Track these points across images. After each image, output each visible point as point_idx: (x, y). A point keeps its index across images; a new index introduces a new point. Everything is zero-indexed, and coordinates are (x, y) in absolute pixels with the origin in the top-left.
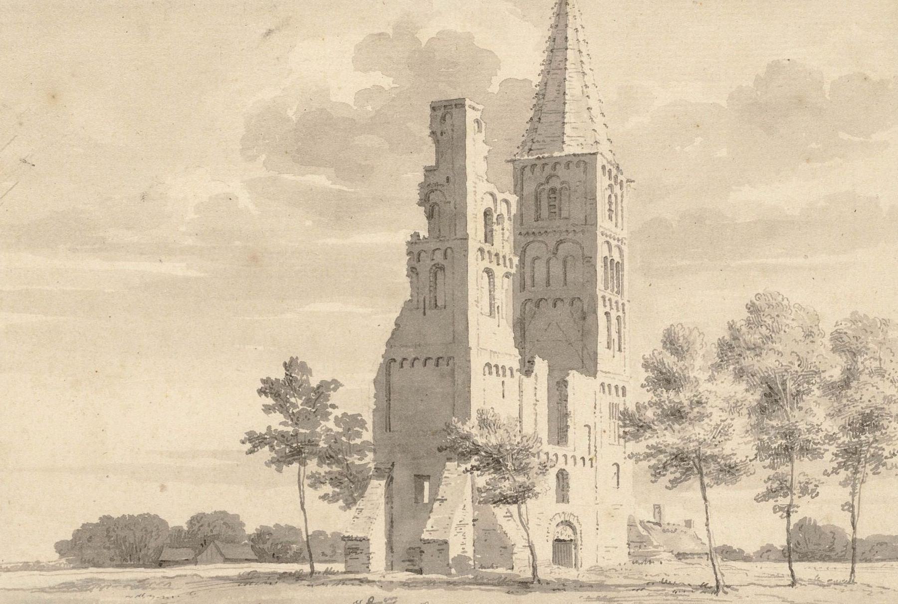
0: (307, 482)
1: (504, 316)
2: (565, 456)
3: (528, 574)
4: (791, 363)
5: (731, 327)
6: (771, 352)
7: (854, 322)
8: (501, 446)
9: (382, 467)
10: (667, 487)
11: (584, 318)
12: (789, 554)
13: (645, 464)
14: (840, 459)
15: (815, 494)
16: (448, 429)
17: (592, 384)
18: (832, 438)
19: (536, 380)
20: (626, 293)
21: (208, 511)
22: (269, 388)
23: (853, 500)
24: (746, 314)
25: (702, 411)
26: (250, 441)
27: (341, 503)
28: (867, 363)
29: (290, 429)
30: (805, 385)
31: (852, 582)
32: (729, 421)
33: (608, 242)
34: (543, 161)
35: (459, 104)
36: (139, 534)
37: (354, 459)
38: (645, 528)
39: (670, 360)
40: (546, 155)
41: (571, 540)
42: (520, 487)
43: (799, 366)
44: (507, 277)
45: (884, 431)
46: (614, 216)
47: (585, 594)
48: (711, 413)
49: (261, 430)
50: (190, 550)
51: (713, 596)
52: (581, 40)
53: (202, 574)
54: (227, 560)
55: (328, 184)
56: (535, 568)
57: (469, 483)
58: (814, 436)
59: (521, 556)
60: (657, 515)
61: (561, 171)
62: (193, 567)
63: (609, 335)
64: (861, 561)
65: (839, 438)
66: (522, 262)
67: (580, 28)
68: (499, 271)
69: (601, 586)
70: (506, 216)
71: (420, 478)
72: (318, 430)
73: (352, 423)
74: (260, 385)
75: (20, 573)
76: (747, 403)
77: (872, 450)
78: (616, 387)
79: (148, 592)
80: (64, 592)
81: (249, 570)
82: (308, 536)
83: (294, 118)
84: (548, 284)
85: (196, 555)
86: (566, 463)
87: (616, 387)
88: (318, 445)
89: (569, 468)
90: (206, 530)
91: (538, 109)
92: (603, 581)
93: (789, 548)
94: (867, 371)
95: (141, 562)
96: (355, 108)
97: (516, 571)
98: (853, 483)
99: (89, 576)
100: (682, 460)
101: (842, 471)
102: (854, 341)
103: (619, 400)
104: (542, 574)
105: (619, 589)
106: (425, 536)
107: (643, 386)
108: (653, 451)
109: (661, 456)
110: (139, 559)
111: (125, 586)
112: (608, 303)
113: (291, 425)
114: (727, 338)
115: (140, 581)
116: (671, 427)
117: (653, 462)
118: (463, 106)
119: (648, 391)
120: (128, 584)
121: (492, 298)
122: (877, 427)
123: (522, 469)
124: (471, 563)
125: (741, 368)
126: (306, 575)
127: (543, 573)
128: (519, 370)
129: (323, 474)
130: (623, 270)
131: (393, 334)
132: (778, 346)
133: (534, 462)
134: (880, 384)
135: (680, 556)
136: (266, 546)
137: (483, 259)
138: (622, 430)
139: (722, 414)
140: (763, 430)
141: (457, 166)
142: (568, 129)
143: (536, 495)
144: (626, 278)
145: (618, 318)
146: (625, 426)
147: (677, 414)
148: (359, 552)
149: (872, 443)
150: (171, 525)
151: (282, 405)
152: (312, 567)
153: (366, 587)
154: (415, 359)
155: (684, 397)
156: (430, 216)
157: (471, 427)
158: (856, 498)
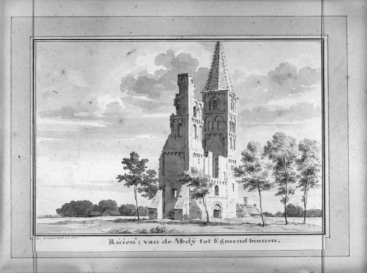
0: (137, 191)
1: (199, 139)
2: (218, 181)
3: (206, 220)
4: (286, 153)
5: (268, 143)
6: (280, 150)
7: (305, 141)
8: (198, 178)
9: (162, 186)
10: (248, 191)
11: (224, 140)
12: (285, 215)
13: (242, 184)
14: (301, 183)
15: (293, 193)
16: (183, 174)
17: (226, 160)
18: (298, 176)
19: (209, 158)
20: (236, 132)
21: (106, 200)
22: (125, 161)
23: (305, 195)
24: (272, 139)
25: (259, 168)
26: (119, 178)
27: (148, 197)
28: (309, 154)
29: (132, 174)
30: (291, 160)
31: (304, 223)
32: (267, 171)
33: (231, 117)
34: (212, 93)
35: (186, 75)
36: (83, 207)
37: (152, 184)
38: (242, 206)
39: (249, 152)
40: (212, 91)
41: (219, 210)
42: (204, 190)
43: (289, 154)
44: (200, 127)
45: (314, 175)
46: (233, 109)
47: (223, 226)
48: (262, 169)
49: (123, 174)
50: (99, 212)
51: (262, 227)
52: (223, 56)
53: (103, 219)
54: (111, 215)
55: (146, 99)
56: (208, 218)
57: (188, 189)
58: (293, 176)
59: (204, 215)
60: (245, 203)
61: (217, 95)
62: (100, 217)
63: (231, 145)
64: (307, 217)
65: (301, 177)
66: (205, 122)
67: (223, 53)
68: (198, 125)
69: (228, 224)
70: (200, 109)
71: (173, 190)
72: (141, 175)
73: (152, 173)
74: (123, 160)
75: (45, 219)
76: (273, 166)
77: (311, 180)
78: (233, 161)
79: (86, 225)
80: (59, 224)
81: (118, 218)
82: (137, 208)
83: (136, 79)
84: (213, 129)
85: (102, 213)
86: (218, 183)
87: (233, 161)
88: (141, 179)
89: (219, 185)
90: (105, 205)
91: (210, 77)
92: (229, 223)
93: (285, 213)
94: (309, 156)
95: (84, 216)
96: (155, 76)
97: (202, 219)
98: (305, 190)
99: (67, 220)
100: (253, 183)
101: (302, 186)
102: (305, 147)
103: (234, 165)
104: (210, 220)
105: (234, 225)
106: (175, 208)
107: (241, 160)
108: (244, 180)
109: (247, 182)
110: (83, 215)
111: (78, 223)
112: (231, 135)
113: (132, 173)
114: (267, 146)
115: (83, 221)
116: (250, 173)
117: (244, 183)
118: (187, 75)
119: (243, 162)
120: (79, 222)
121: (196, 133)
122: (312, 173)
123: (204, 185)
124: (189, 217)
125: (271, 155)
126: (137, 220)
127: (211, 220)
128: (204, 155)
129: (142, 188)
130: (235, 125)
131: (165, 145)
132: (282, 149)
133: (208, 183)
134: (313, 160)
135: (252, 215)
136: (124, 211)
137: (193, 122)
138: (235, 174)
139: (265, 169)
140: (278, 174)
141: (186, 93)
142: (219, 83)
143: (209, 193)
144: (236, 128)
145: (234, 140)
146: (236, 172)
147: (251, 169)
148: (154, 213)
149: (311, 178)
150: (93, 204)
151: (129, 167)
152: (139, 217)
153: (156, 224)
154: (172, 153)
155: (254, 164)
156: (177, 108)
157: (189, 172)
158: (306, 195)
